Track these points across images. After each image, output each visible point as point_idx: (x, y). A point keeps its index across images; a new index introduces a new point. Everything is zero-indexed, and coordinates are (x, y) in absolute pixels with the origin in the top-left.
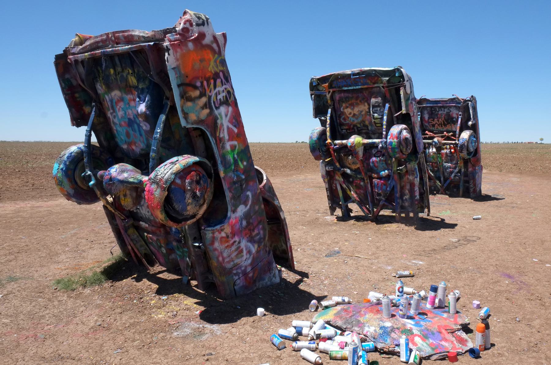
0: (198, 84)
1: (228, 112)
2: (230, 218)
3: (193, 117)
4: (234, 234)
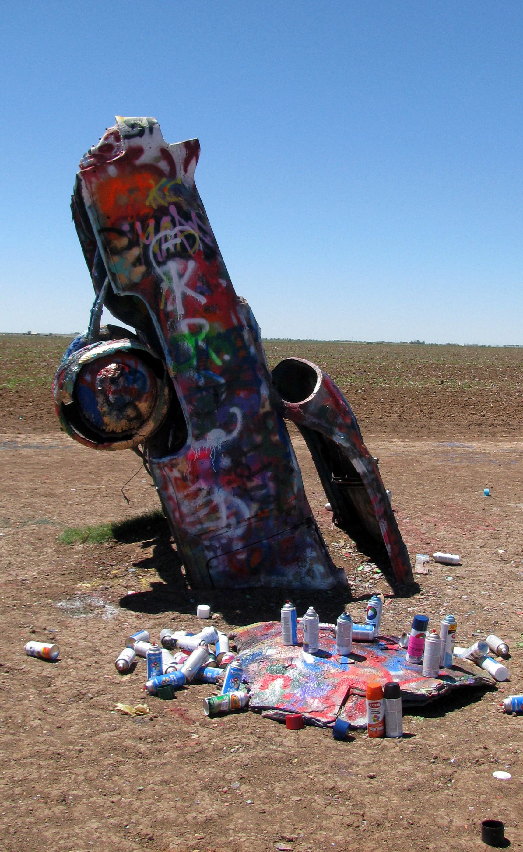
0: (126, 227)
1: (185, 269)
2: (189, 447)
3: (123, 279)
4: (196, 476)
